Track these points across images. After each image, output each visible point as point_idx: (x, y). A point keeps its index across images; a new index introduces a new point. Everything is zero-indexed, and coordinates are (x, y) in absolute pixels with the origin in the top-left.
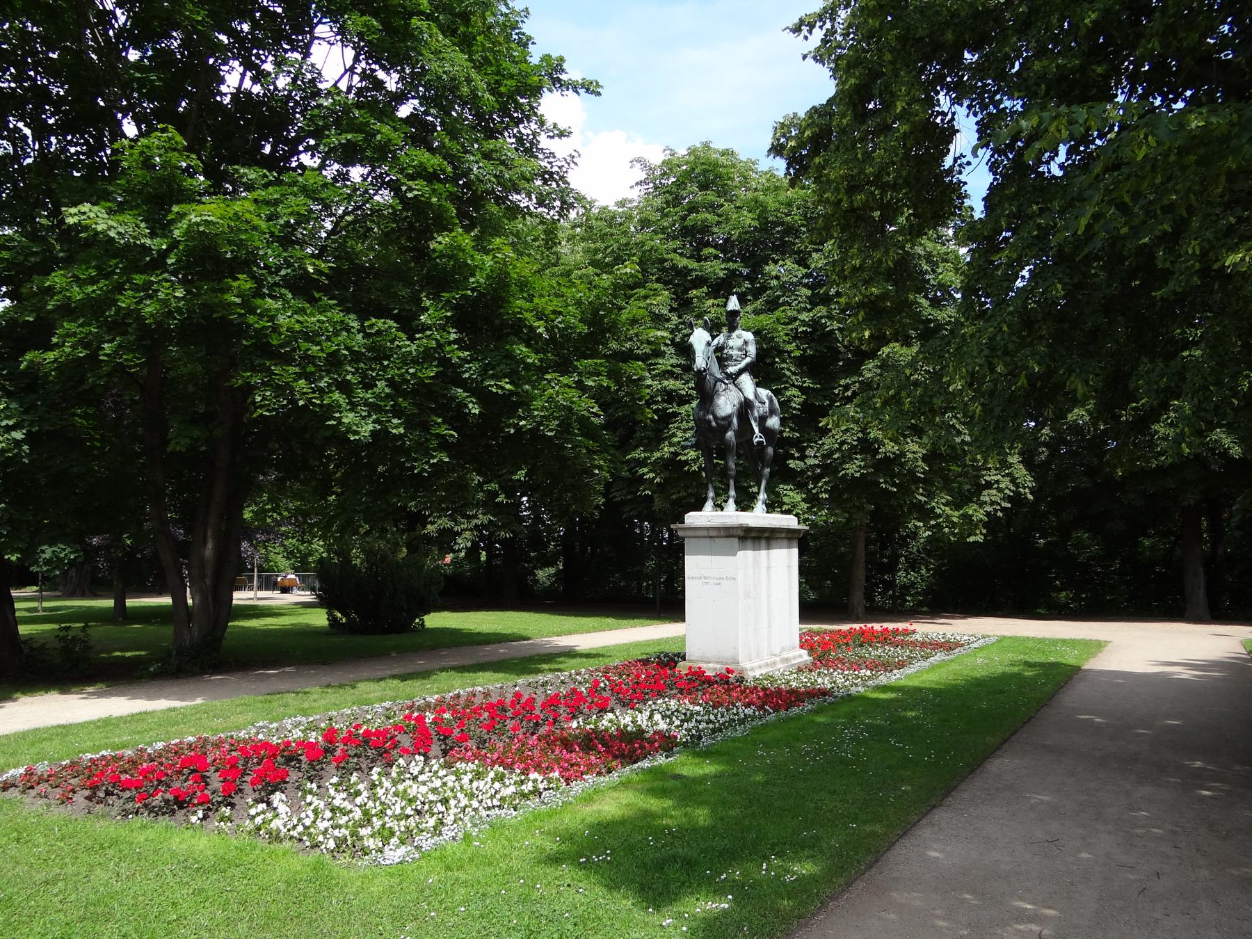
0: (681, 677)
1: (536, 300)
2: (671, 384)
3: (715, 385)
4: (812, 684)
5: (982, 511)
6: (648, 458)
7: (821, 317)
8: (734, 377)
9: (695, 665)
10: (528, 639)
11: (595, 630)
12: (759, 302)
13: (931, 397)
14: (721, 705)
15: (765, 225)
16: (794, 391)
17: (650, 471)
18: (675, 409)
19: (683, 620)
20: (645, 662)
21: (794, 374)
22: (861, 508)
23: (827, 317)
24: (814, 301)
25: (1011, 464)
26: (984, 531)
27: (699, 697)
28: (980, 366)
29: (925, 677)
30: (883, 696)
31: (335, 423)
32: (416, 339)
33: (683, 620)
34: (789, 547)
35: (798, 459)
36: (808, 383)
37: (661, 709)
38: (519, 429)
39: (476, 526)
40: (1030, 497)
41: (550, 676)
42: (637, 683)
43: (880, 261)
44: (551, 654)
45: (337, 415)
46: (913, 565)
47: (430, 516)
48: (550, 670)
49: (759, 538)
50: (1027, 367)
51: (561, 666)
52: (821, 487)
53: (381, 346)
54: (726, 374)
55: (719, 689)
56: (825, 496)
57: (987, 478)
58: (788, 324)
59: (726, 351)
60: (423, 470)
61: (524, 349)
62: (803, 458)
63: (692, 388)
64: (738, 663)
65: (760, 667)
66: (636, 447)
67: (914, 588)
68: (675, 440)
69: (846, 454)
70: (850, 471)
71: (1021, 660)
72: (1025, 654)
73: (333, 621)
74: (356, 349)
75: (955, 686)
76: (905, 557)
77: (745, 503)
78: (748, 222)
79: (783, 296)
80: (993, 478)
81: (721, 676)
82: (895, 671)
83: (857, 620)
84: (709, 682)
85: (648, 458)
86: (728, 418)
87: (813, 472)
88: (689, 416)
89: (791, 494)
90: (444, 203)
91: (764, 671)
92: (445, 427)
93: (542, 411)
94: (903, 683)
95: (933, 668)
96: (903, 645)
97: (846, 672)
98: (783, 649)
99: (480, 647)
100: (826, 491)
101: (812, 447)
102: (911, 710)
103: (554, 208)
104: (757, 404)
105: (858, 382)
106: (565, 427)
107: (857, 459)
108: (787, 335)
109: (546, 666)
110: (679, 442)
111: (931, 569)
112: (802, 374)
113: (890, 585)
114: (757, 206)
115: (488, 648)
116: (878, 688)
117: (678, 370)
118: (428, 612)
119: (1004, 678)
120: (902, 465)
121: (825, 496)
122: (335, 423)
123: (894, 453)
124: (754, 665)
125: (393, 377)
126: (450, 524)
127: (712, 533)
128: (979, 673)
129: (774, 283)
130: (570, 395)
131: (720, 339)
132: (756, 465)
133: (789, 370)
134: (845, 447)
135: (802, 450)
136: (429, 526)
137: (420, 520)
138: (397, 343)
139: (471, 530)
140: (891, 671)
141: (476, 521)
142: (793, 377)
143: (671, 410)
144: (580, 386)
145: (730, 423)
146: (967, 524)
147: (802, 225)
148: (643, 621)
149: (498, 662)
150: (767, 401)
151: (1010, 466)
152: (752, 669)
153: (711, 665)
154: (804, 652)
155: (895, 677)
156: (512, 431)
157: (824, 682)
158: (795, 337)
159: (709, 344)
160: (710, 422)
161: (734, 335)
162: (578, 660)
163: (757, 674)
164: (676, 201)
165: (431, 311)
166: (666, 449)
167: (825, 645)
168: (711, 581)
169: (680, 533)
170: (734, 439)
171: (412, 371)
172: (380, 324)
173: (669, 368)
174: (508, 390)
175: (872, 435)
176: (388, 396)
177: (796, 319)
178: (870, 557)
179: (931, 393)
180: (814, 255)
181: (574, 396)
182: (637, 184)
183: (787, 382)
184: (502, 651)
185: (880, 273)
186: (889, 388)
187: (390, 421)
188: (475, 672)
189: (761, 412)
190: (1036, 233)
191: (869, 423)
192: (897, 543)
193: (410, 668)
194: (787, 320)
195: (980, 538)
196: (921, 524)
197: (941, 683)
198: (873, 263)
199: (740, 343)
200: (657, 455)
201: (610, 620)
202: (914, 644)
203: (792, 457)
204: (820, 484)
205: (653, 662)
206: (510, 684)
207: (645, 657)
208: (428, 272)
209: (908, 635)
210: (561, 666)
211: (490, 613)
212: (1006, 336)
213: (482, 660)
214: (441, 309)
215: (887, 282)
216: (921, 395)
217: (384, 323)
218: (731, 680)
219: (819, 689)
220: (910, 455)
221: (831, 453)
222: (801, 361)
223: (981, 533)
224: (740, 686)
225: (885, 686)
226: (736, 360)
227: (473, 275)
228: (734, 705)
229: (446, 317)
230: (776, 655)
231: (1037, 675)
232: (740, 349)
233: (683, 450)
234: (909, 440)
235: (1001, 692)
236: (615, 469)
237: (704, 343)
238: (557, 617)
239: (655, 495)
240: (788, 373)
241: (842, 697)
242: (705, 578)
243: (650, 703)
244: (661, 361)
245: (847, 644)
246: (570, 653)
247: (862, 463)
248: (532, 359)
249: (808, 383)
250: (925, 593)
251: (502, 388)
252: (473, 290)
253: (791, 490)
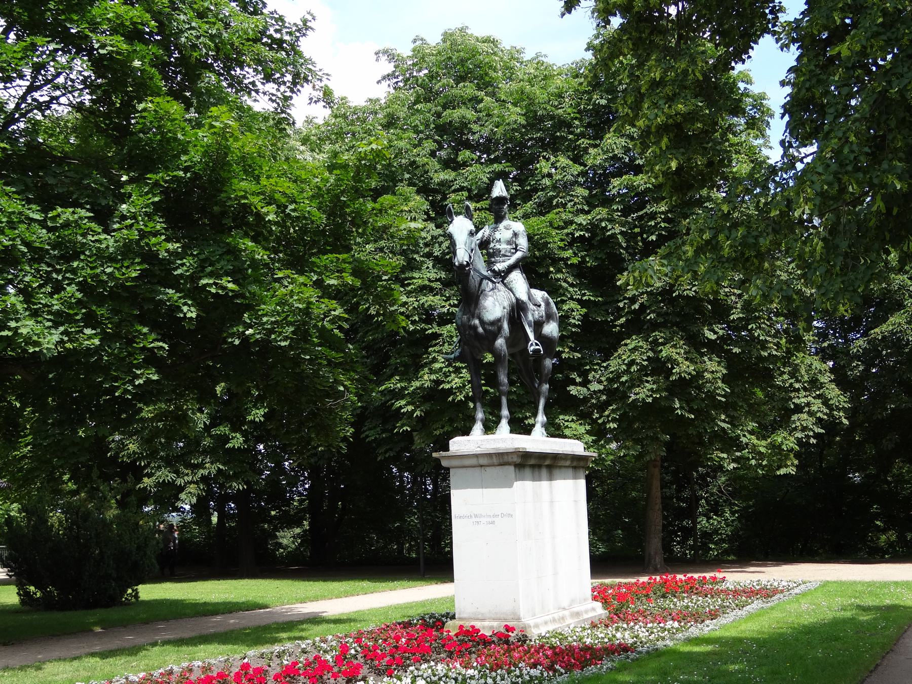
0: (450, 638)
1: (264, 181)
2: (429, 300)
3: (480, 284)
4: (610, 640)
5: (792, 439)
6: (405, 388)
7: (601, 220)
8: (502, 276)
9: (467, 625)
10: (266, 607)
11: (347, 594)
12: (528, 205)
13: (756, 238)
14: (499, 666)
15: (534, 121)
16: (573, 305)
17: (408, 404)
18: (434, 329)
19: (452, 580)
20: (407, 625)
21: (572, 285)
22: (655, 439)
23: (609, 220)
24: (591, 203)
25: (822, 383)
26: (796, 462)
27: (473, 660)
28: (829, 184)
29: (743, 627)
30: (697, 649)
31: (10, 334)
32: (115, 230)
33: (452, 580)
34: (575, 478)
35: (581, 384)
36: (588, 296)
37: (425, 675)
38: (245, 339)
39: (204, 479)
40: (845, 421)
41: (288, 645)
42: (396, 647)
43: (685, 72)
44: (292, 622)
45: (13, 324)
46: (715, 509)
47: (146, 467)
48: (290, 639)
49: (539, 466)
50: (886, 184)
51: (303, 634)
52: (608, 416)
53: (70, 241)
54: (494, 271)
55: (500, 649)
56: (613, 425)
57: (796, 401)
58: (563, 228)
59: (492, 245)
60: (126, 391)
61: (250, 244)
62: (585, 383)
63: (455, 306)
64: (519, 619)
65: (546, 623)
66: (392, 376)
67: (718, 534)
68: (437, 366)
69: (636, 375)
70: (642, 396)
71: (853, 604)
72: (856, 598)
73: (26, 597)
74: (37, 245)
75: (781, 635)
76: (706, 499)
77: (521, 427)
78: (513, 118)
79: (555, 197)
80: (803, 400)
81: (499, 635)
82: (707, 622)
83: (656, 571)
84: (485, 641)
85: (405, 388)
86: (497, 322)
87: (598, 398)
88: (451, 337)
89: (573, 425)
90: (148, 69)
91: (551, 627)
92: (153, 336)
93: (273, 316)
94: (718, 634)
95: (751, 617)
96: (715, 594)
97: (649, 625)
98: (573, 601)
99: (204, 619)
100: (614, 420)
101: (595, 371)
102: (733, 663)
103: (284, 83)
104: (531, 306)
105: (647, 292)
106: (302, 335)
107: (648, 382)
108: (562, 240)
109: (284, 635)
110: (441, 369)
111: (736, 512)
112: (581, 286)
113: (688, 532)
114: (521, 98)
115: (219, 618)
116: (690, 641)
117: (437, 285)
118: (143, 582)
119: (836, 623)
120: (699, 388)
121: (613, 425)
122: (10, 334)
123: (690, 374)
124: (539, 621)
125: (85, 281)
126: (171, 476)
127: (483, 461)
128: (807, 620)
129: (547, 182)
130: (308, 295)
131: (486, 232)
132: (533, 382)
133: (565, 281)
134: (634, 368)
135: (584, 374)
136: (146, 480)
137: (135, 471)
138: (90, 237)
139: (196, 483)
140: (703, 621)
141: (202, 471)
142: (571, 289)
143: (430, 331)
144: (318, 284)
145: (500, 328)
146: (776, 454)
147: (576, 118)
148: (405, 583)
149: (226, 633)
150: (543, 304)
151: (822, 386)
152: (537, 626)
153: (486, 623)
154: (598, 605)
155: (709, 628)
156: (237, 342)
157: (624, 636)
158: (573, 242)
159: (471, 234)
160: (475, 328)
161: (501, 226)
162: (325, 626)
163: (543, 631)
164: (428, 95)
165: (134, 197)
166: (426, 377)
167: (621, 597)
168: (483, 520)
169: (444, 463)
170: (505, 348)
171: (109, 270)
172: (67, 214)
173: (427, 283)
174: (232, 291)
175: (664, 354)
176: (79, 302)
177: (571, 222)
178: (666, 500)
179: (755, 233)
180: (592, 151)
181: (311, 296)
182: (384, 78)
183: (564, 295)
184: (233, 621)
185: (686, 88)
186: (702, 231)
187: (81, 332)
188: (195, 645)
189: (536, 316)
190: (880, 20)
191: (679, 277)
192: (696, 483)
193: (115, 644)
194: (562, 224)
195: (792, 471)
196: (725, 456)
197: (763, 633)
198: (677, 75)
199: (508, 235)
200: (416, 384)
201: (365, 584)
202: (726, 592)
203: (574, 383)
204: (607, 413)
205: (416, 625)
206: (238, 656)
207: (406, 620)
208: (130, 151)
209: (717, 583)
210: (303, 634)
211: (221, 581)
212: (855, 148)
213: (205, 632)
214: (147, 194)
215: (696, 97)
216: (743, 237)
217: (74, 213)
218: (511, 639)
219: (620, 645)
220: (707, 375)
221: (619, 375)
222: (579, 271)
223: (793, 464)
224: (522, 646)
225: (697, 639)
226: (504, 256)
227: (186, 152)
228: (516, 666)
229: (153, 203)
230: (564, 609)
231: (874, 619)
232: (509, 242)
233: (447, 377)
234: (706, 359)
235: (837, 639)
236: (364, 390)
237: (466, 233)
238: (307, 583)
239: (415, 434)
240: (565, 285)
241: (648, 652)
242: (476, 516)
243: (411, 668)
244: (416, 275)
245: (647, 596)
246: (316, 620)
247: (655, 387)
248: (261, 255)
249: (588, 296)
250: (731, 539)
251: (224, 288)
252: (186, 170)
253: (573, 421)
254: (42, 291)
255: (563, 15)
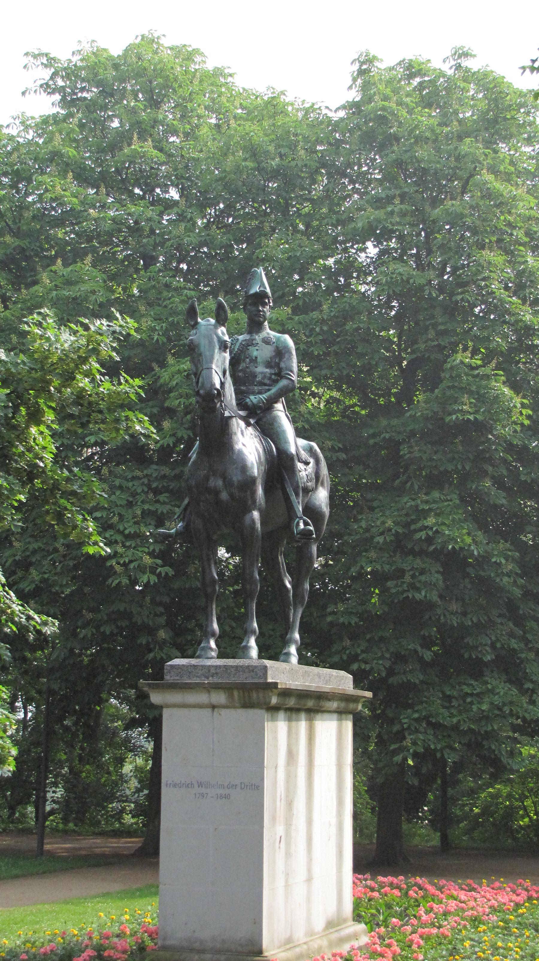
226: (262, 384)
242: (200, 785)
254: (333, 650)
255: (475, 56)
